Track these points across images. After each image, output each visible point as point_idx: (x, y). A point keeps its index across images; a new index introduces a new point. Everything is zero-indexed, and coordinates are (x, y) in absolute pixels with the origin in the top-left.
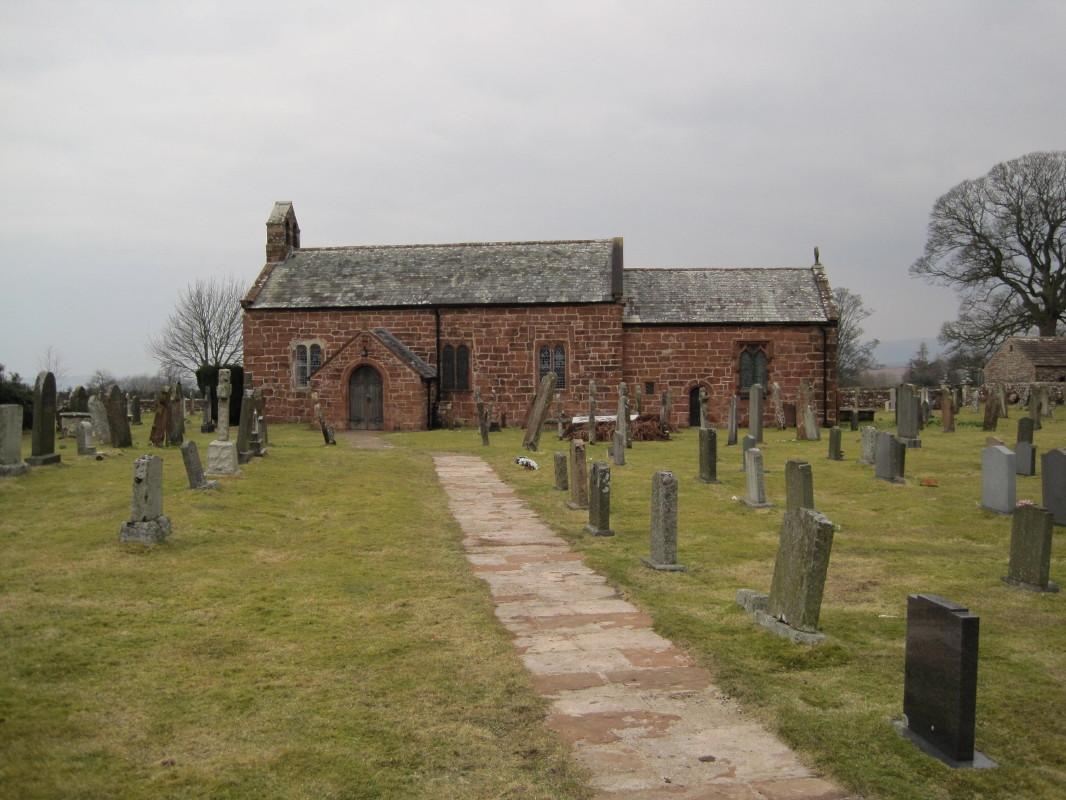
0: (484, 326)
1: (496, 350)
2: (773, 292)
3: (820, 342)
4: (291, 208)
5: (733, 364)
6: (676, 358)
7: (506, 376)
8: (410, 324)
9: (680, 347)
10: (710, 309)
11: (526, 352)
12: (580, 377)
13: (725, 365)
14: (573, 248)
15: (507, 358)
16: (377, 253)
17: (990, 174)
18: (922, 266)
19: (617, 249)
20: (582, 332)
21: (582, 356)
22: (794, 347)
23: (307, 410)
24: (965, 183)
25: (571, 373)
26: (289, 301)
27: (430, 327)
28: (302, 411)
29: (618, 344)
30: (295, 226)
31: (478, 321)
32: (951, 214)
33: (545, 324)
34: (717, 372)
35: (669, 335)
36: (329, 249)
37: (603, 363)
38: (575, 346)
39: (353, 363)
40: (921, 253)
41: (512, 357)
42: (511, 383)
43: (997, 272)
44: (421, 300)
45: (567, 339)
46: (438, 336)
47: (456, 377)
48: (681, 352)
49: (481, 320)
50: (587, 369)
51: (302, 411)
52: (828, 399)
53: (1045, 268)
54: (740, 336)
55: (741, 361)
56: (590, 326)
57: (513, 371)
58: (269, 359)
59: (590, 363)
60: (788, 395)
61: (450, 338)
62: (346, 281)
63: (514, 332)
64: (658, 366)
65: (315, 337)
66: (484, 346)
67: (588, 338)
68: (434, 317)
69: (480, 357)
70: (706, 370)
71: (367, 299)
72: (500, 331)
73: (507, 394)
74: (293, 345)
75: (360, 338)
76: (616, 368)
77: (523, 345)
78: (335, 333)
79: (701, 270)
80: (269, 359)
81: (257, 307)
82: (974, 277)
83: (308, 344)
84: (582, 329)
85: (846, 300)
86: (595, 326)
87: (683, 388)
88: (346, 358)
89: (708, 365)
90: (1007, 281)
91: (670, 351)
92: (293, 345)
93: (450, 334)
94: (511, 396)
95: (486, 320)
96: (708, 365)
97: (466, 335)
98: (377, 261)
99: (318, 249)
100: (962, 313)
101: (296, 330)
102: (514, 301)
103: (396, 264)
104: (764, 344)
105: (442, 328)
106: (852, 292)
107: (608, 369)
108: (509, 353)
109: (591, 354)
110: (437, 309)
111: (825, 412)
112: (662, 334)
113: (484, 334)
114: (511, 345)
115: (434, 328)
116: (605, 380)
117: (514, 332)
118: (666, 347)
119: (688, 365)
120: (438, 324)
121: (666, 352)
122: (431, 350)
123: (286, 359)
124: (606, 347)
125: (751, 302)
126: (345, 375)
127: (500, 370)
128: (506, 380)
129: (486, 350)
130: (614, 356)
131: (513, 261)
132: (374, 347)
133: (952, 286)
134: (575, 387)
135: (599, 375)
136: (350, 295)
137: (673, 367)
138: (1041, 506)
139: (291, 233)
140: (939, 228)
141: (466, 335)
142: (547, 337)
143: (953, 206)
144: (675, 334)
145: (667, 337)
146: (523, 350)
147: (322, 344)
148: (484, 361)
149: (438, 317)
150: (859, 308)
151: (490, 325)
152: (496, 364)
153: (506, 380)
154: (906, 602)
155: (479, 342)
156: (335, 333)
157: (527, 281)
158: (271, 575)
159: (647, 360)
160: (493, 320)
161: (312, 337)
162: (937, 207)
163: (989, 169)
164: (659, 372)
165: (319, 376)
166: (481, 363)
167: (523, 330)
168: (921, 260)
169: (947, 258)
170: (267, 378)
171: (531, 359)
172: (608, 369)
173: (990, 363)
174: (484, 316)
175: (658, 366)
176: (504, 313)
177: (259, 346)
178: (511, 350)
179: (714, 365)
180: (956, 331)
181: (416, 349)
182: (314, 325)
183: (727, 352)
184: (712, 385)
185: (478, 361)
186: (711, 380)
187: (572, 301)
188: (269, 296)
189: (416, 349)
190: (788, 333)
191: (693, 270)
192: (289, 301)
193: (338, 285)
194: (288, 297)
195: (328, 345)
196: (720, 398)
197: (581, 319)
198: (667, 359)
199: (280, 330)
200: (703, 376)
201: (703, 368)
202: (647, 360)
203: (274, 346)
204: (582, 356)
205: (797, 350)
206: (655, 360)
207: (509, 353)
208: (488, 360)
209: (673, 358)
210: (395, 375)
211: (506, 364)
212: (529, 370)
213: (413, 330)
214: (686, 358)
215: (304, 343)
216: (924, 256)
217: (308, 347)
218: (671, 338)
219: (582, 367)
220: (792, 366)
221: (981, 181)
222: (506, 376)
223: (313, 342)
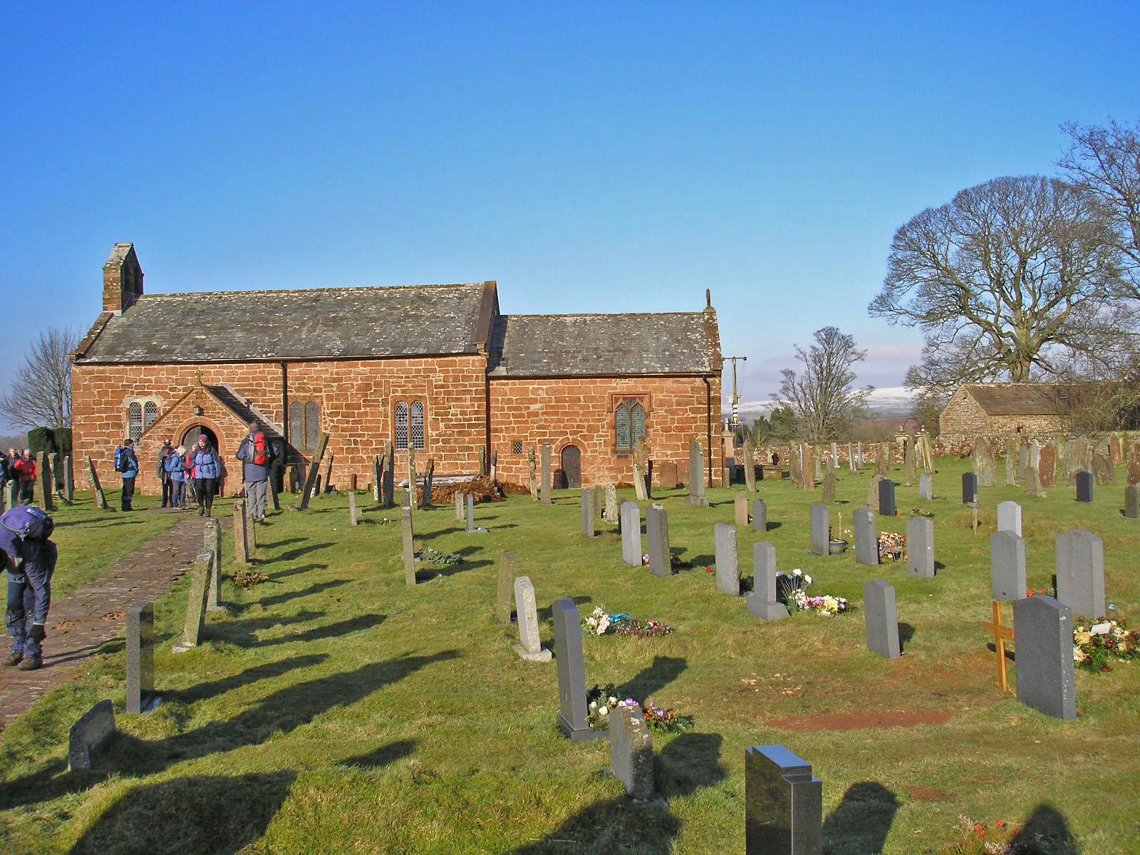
0: (334, 380)
1: (348, 406)
2: (658, 339)
3: (703, 394)
4: (132, 250)
5: (609, 418)
6: (546, 413)
7: (360, 436)
8: (254, 379)
9: (550, 402)
10: (585, 360)
11: (381, 409)
12: (440, 435)
13: (599, 420)
14: (439, 292)
15: (360, 415)
16: (226, 299)
17: (955, 201)
18: (883, 304)
19: (490, 294)
20: (442, 387)
21: (442, 414)
22: (674, 399)
24: (928, 211)
25: (430, 431)
26: (123, 354)
27: (275, 382)
29: (480, 399)
30: (137, 270)
31: (328, 376)
32: (911, 245)
33: (402, 377)
34: (590, 428)
35: (538, 389)
36: (174, 295)
37: (465, 420)
38: (435, 401)
40: (879, 289)
41: (366, 413)
42: (363, 443)
43: (964, 310)
44: (266, 353)
45: (426, 394)
46: (285, 392)
48: (553, 407)
49: (332, 374)
50: (447, 427)
52: (712, 457)
53: (1017, 305)
54: (615, 388)
55: (616, 416)
56: (451, 380)
57: (367, 429)
58: (100, 418)
59: (450, 420)
60: (669, 452)
61: (297, 394)
62: (188, 330)
63: (368, 387)
64: (527, 422)
65: (150, 393)
66: (335, 402)
67: (449, 393)
68: (280, 370)
69: (331, 414)
70: (578, 426)
71: (208, 351)
72: (352, 385)
73: (361, 454)
74: (127, 402)
75: (193, 395)
76: (479, 424)
77: (378, 401)
78: (172, 389)
79: (581, 315)
80: (100, 418)
82: (931, 317)
83: (142, 401)
84: (442, 383)
85: (836, 340)
86: (456, 379)
87: (554, 447)
88: (178, 417)
89: (581, 420)
90: (977, 321)
91: (538, 406)
92: (127, 402)
93: (298, 390)
95: (337, 373)
96: (581, 420)
97: (315, 390)
98: (224, 309)
99: (161, 296)
100: (926, 355)
101: (130, 386)
103: (245, 311)
104: (640, 396)
105: (289, 383)
106: (843, 331)
107: (470, 426)
108: (363, 410)
109: (452, 411)
111: (710, 471)
112: (531, 387)
113: (335, 389)
114: (364, 401)
115: (281, 382)
116: (467, 439)
117: (368, 387)
118: (535, 401)
119: (560, 421)
120: (285, 373)
121: (533, 407)
122: (277, 407)
123: (119, 418)
124: (468, 403)
125: (631, 351)
127: (352, 429)
128: (359, 439)
129: (337, 407)
130: (476, 413)
131: (373, 308)
132: (209, 404)
133: (918, 325)
134: (435, 446)
135: (460, 433)
136: (189, 346)
138: (49, 539)
139: (132, 279)
140: (898, 262)
141: (315, 390)
142: (403, 391)
143: (915, 236)
144: (544, 387)
146: (378, 406)
147: (159, 402)
148: (335, 419)
150: (850, 350)
151: (340, 380)
152: (348, 422)
153: (359, 439)
155: (329, 398)
156: (172, 389)
157: (385, 330)
158: (866, 844)
159: (514, 416)
160: (345, 373)
162: (896, 238)
163: (953, 195)
164: (527, 429)
165: (149, 437)
166: (333, 421)
167: (378, 384)
168: (882, 298)
169: (908, 296)
170: (97, 438)
171: (386, 416)
172: (470, 426)
173: (944, 413)
174: (334, 368)
175: (527, 422)
176: (356, 366)
178: (364, 406)
179: (587, 421)
180: (923, 376)
181: (260, 406)
182: (150, 381)
183: (601, 406)
184: (586, 443)
185: (328, 419)
186: (584, 437)
187: (430, 352)
188: (101, 348)
189: (260, 406)
191: (574, 315)
192: (123, 354)
193: (179, 337)
194: (123, 349)
195: (165, 403)
196: (595, 458)
197: (440, 371)
198: (536, 414)
199: (112, 386)
200: (576, 433)
201: (575, 424)
202: (514, 416)
203: (106, 403)
204: (442, 414)
205: (678, 404)
206: (522, 416)
207: (363, 410)
208: (340, 418)
209: (543, 413)
211: (360, 422)
213: (257, 385)
214: (557, 413)
215: (138, 400)
216: (885, 292)
217: (143, 406)
219: (442, 425)
220: (673, 421)
221: (945, 209)
222: (360, 436)
223: (147, 399)
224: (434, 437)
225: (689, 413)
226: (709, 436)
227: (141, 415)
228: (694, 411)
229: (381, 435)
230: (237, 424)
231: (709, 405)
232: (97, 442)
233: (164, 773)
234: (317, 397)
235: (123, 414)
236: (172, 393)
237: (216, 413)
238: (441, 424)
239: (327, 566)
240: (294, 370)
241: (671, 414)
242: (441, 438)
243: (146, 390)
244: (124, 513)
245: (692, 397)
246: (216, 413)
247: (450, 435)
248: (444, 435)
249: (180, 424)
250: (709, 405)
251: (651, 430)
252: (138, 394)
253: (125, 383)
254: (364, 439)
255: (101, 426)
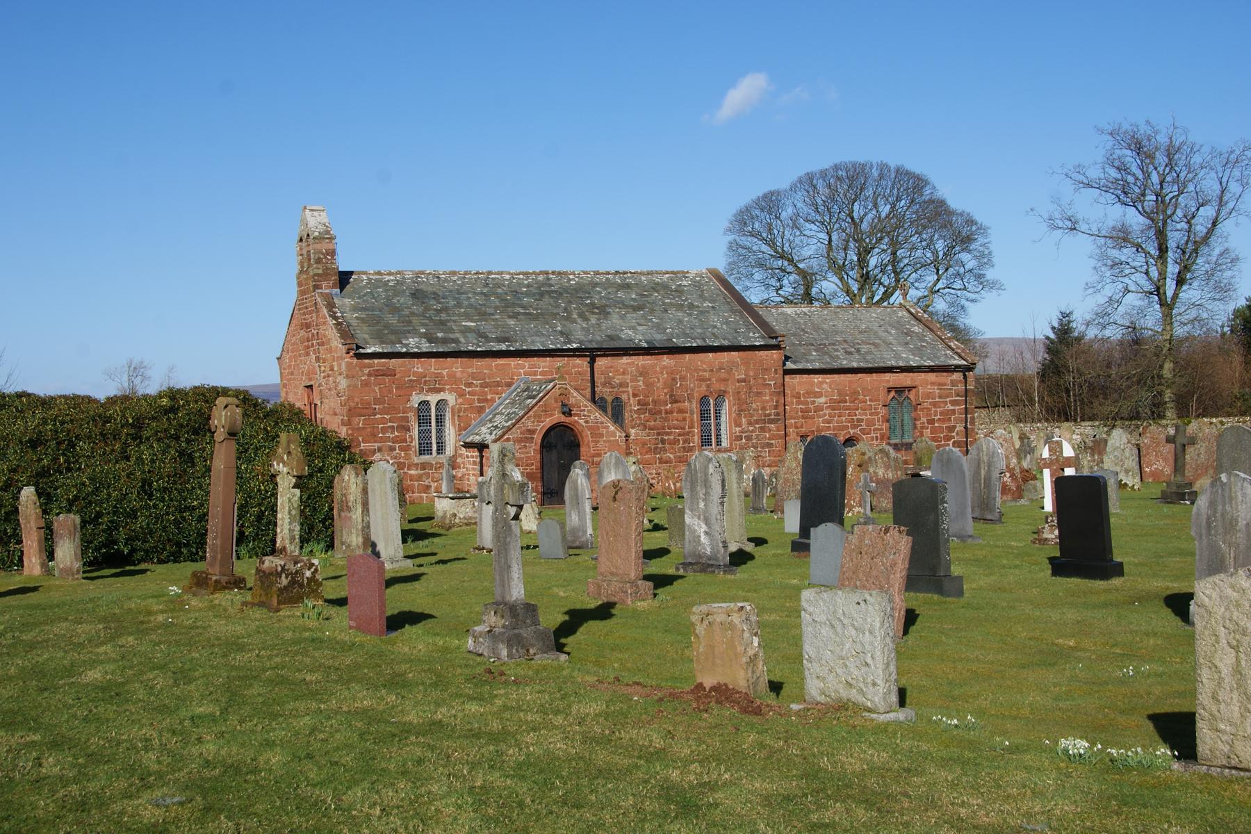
20: (744, 380)
23: (434, 485)
28: (428, 487)
29: (779, 393)
39: (548, 422)
47: (983, 481)
50: (750, 424)
51: (428, 487)
74: (416, 400)
78: (469, 385)
80: (383, 421)
81: (369, 351)
83: (433, 399)
93: (604, 385)
94: (671, 456)
96: (860, 414)
97: (621, 385)
102: (667, 345)
110: (592, 354)
123: (406, 419)
126: (538, 437)
128: (666, 438)
134: (738, 443)
137: (827, 417)
145: (821, 383)
147: (451, 398)
149: (592, 363)
153: (666, 438)
154: (1150, 726)
161: (438, 391)
174: (641, 361)
177: (369, 403)
186: (863, 431)
190: (932, 377)
195: (460, 400)
210: (597, 435)
211: (666, 420)
212: (691, 427)
215: (428, 398)
218: (825, 386)
224: (738, 434)
225: (949, 405)
226: (966, 428)
227: (430, 416)
228: (954, 403)
229: (688, 433)
230: (602, 423)
231: (966, 397)
232: (380, 450)
233: (1109, 484)
234: (624, 392)
235: (411, 415)
236: (467, 390)
237: (581, 411)
238: (744, 420)
239: (610, 605)
240: (601, 363)
241: (935, 406)
242: (744, 435)
243: (437, 386)
244: (92, 585)
245: (950, 389)
246: (581, 411)
247: (752, 431)
248: (746, 432)
249: (542, 424)
250: (966, 397)
251: (918, 423)
252: (429, 390)
253: (412, 378)
254: (672, 437)
255: (384, 430)
